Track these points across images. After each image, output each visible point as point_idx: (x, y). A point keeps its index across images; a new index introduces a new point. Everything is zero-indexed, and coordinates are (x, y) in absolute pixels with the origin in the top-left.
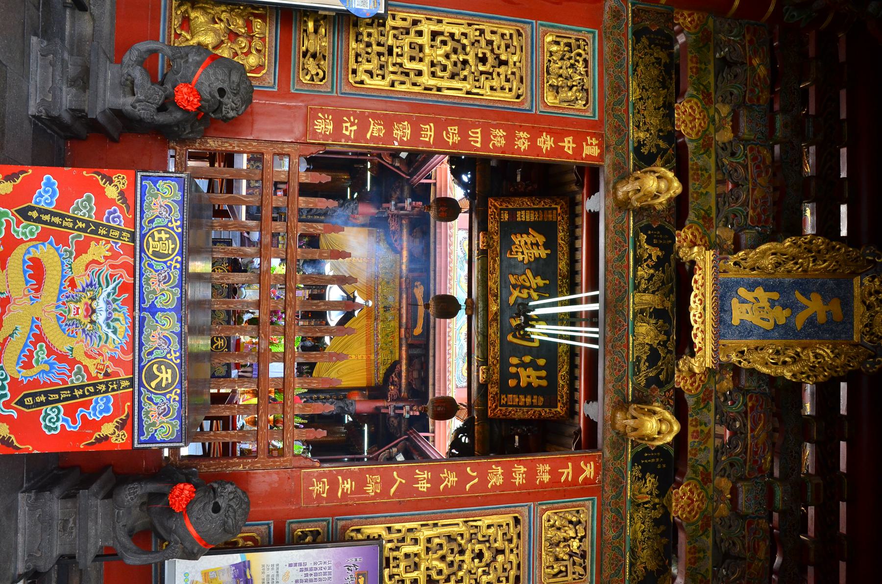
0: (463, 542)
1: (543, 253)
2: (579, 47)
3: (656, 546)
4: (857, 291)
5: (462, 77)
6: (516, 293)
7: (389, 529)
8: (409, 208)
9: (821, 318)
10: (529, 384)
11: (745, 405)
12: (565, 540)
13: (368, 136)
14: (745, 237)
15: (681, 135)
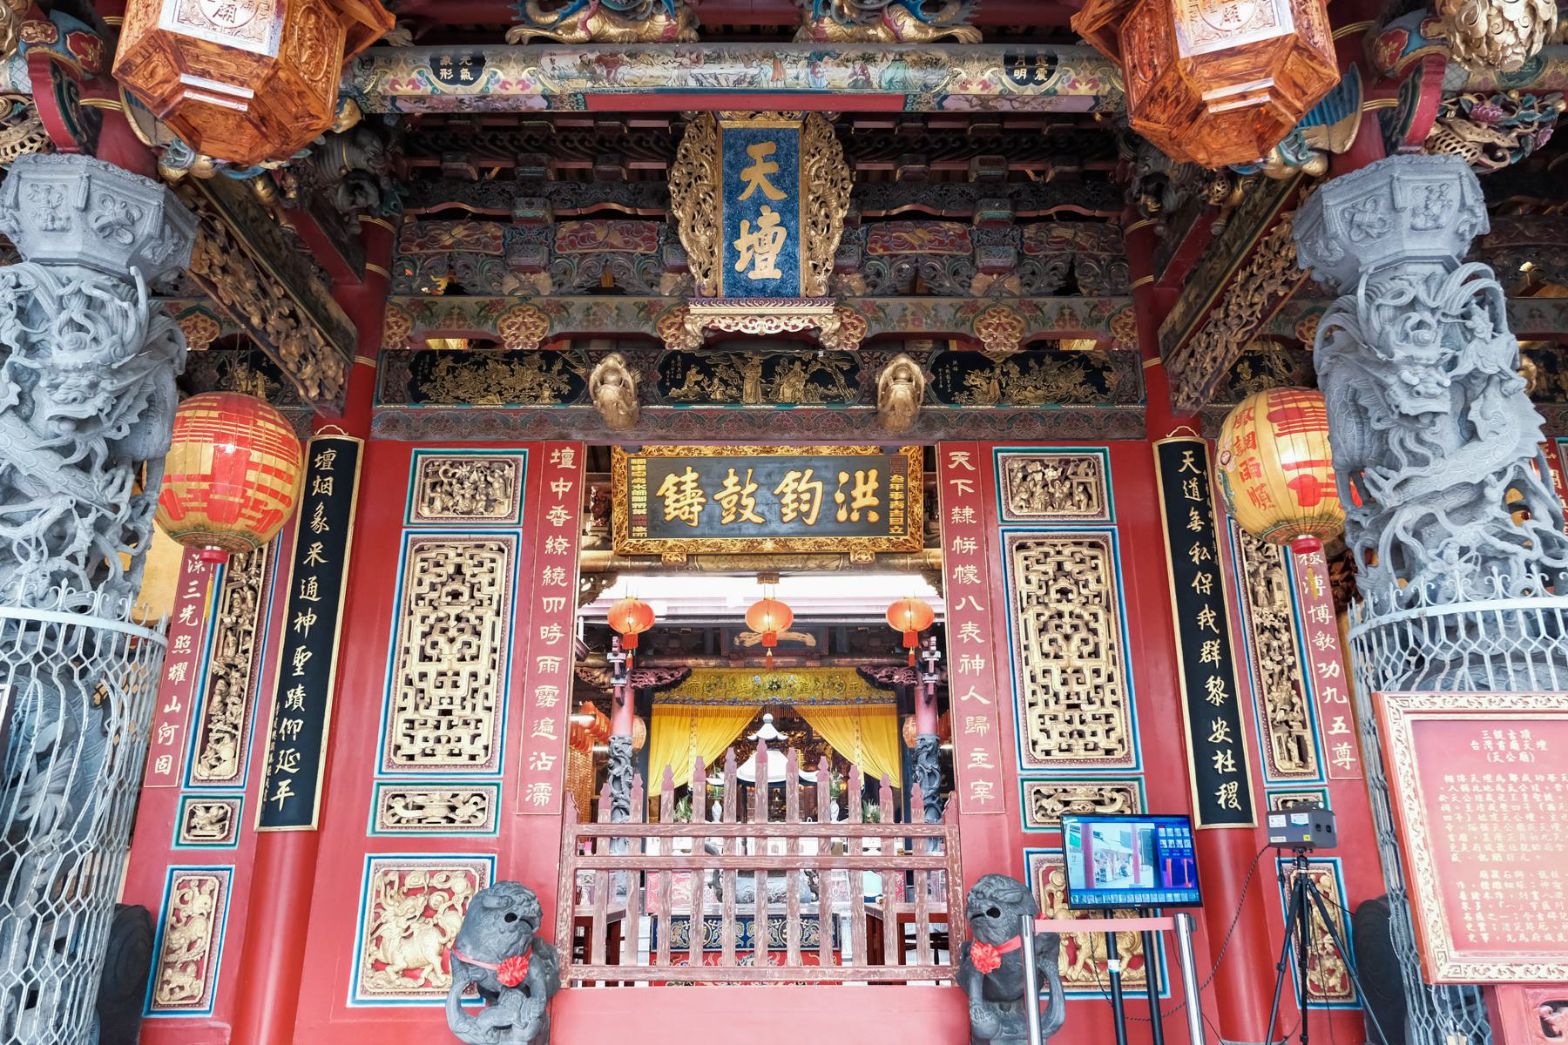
0: (1047, 614)
1: (690, 476)
2: (436, 472)
3: (1055, 371)
4: (738, 124)
5: (477, 622)
6: (747, 514)
7: (1031, 705)
8: (622, 656)
9: (772, 168)
10: (875, 494)
11: (881, 257)
12: (1045, 486)
13: (554, 738)
14: (672, 259)
15: (544, 342)
